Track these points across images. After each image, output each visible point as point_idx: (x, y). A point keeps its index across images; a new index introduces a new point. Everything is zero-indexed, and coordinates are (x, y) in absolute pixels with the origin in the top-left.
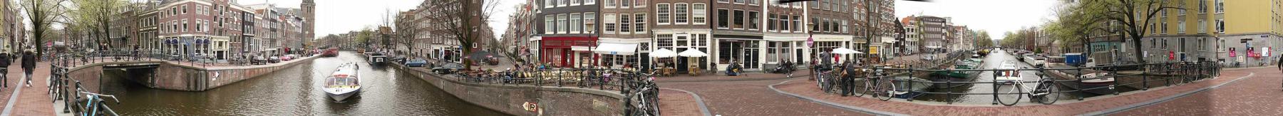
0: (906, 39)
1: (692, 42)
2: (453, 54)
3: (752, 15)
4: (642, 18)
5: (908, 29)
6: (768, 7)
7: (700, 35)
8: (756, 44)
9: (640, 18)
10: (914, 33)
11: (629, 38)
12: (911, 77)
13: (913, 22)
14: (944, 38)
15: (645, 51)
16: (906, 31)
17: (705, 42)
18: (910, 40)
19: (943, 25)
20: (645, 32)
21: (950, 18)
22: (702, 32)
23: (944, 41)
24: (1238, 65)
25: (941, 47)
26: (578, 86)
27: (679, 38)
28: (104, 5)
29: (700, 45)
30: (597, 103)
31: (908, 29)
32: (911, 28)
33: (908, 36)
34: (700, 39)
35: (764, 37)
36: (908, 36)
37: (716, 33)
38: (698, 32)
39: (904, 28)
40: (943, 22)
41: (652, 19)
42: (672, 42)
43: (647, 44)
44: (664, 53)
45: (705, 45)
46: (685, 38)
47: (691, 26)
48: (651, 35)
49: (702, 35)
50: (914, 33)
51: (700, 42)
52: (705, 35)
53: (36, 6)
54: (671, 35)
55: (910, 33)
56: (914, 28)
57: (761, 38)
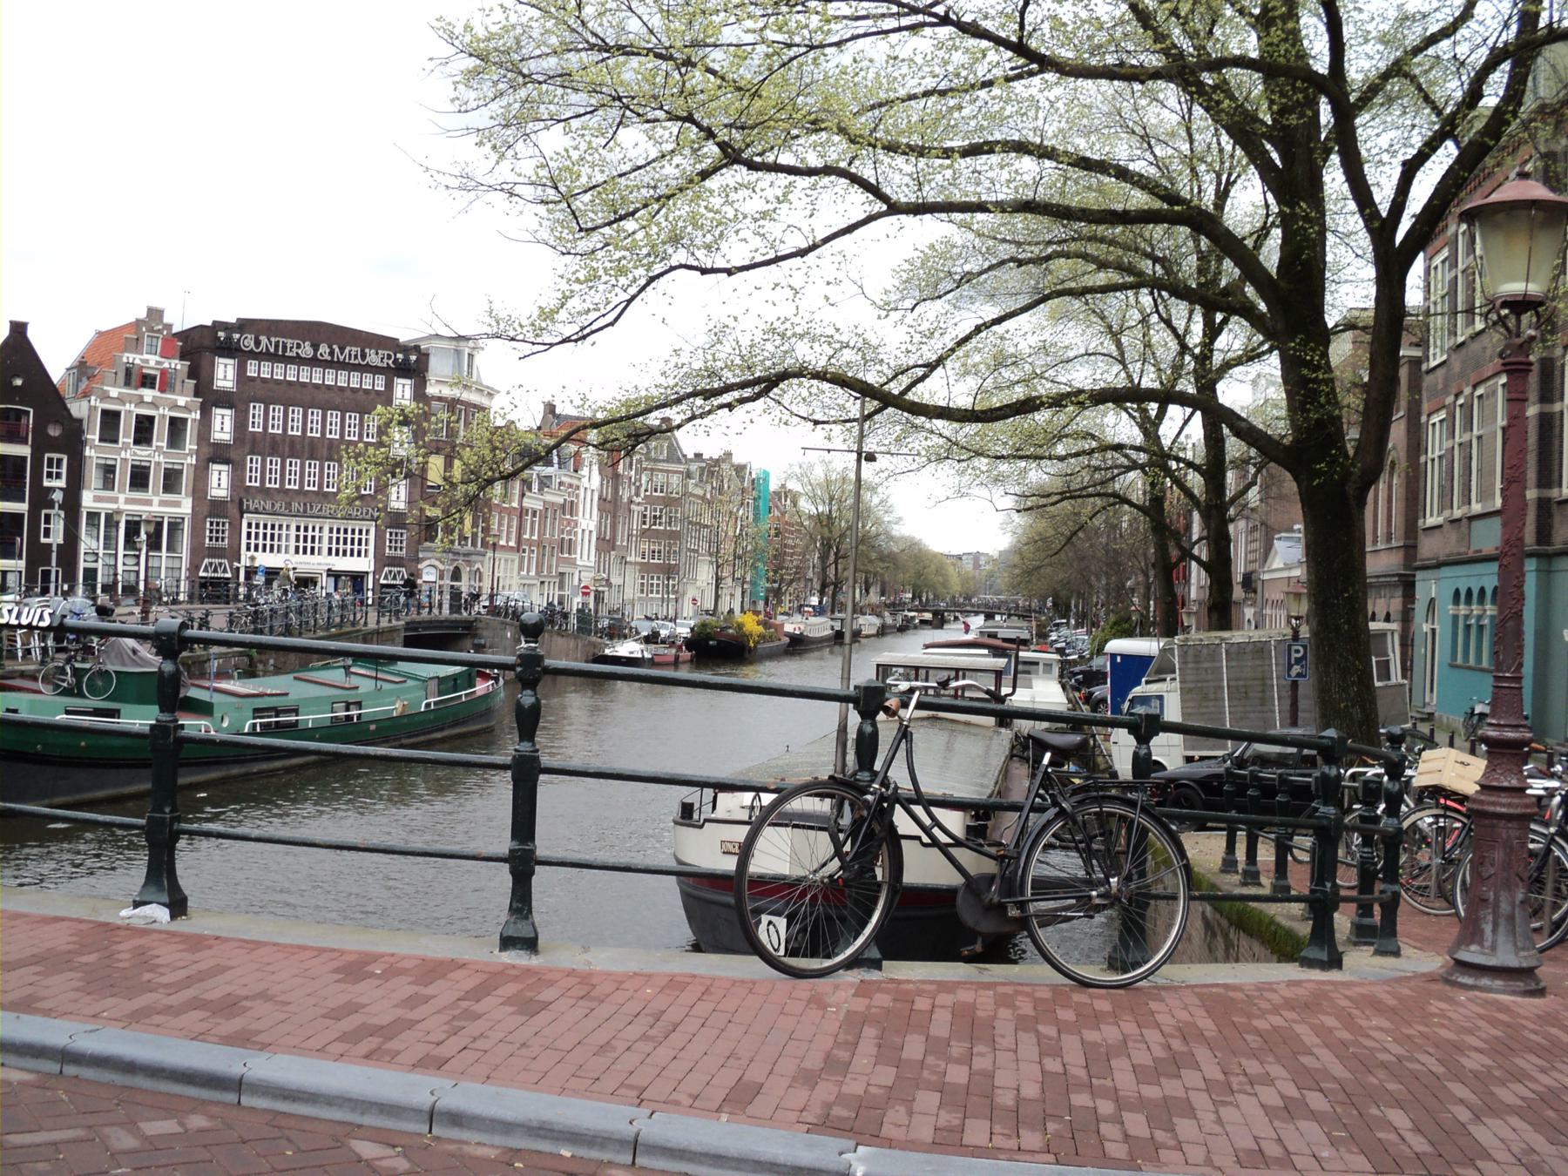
0: (88, 500)
2: (1543, 1071)
5: (110, 420)
10: (156, 455)
13: (150, 361)
14: (398, 497)
16: (93, 436)
18: (124, 502)
19: (403, 390)
21: (155, 314)
23: (397, 520)
24: (1290, 667)
25: (364, 564)
28: (455, 183)
30: (367, 1149)
31: (110, 420)
32: (129, 412)
33: (108, 471)
36: (108, 471)
39: (78, 409)
40: (404, 370)
50: (156, 455)
53: (757, 389)
55: (127, 453)
56: (162, 414)
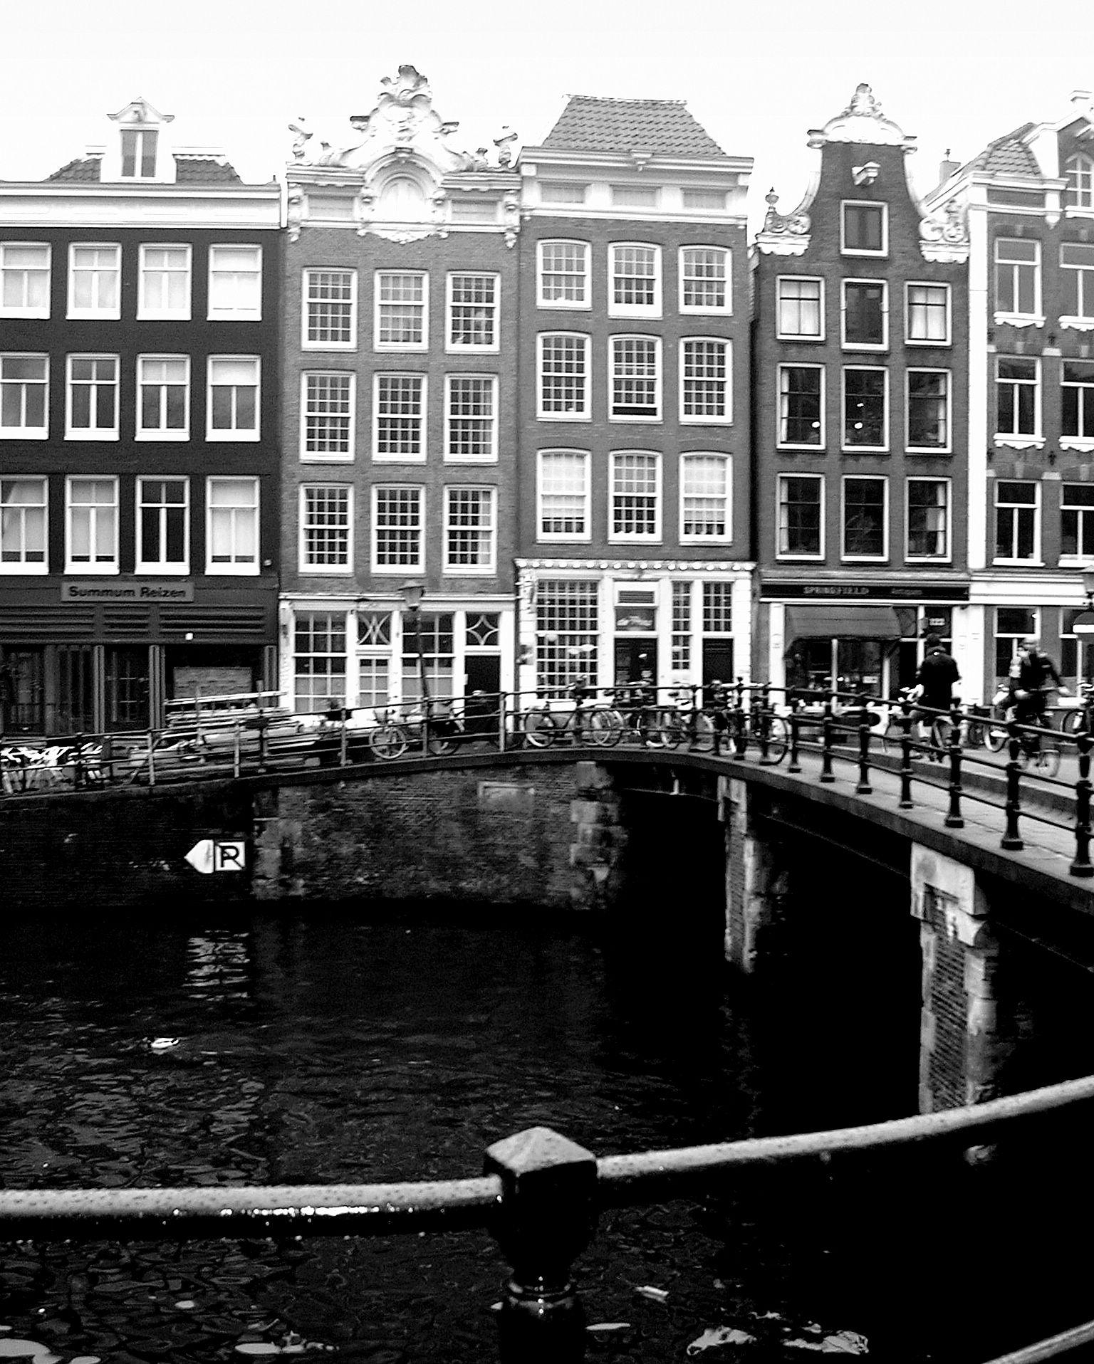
1: (676, 613)
3: (923, 497)
4: (476, 509)
6: (990, 455)
7: (707, 586)
8: (938, 622)
9: (466, 508)
11: (989, 261)
12: (579, 703)
15: (482, 650)
17: (728, 614)
20: (487, 568)
22: (716, 572)
26: (421, 286)
27: (625, 596)
29: (707, 627)
34: (707, 601)
35: (974, 588)
37: (773, 576)
38: (700, 575)
41: (517, 518)
42: (594, 613)
43: (493, 618)
44: (396, 670)
45: (728, 627)
46: (649, 596)
47: (669, 552)
48: (509, 581)
49: (718, 586)
51: (706, 614)
52: (728, 587)
54: (594, 586)
57: (961, 593)
